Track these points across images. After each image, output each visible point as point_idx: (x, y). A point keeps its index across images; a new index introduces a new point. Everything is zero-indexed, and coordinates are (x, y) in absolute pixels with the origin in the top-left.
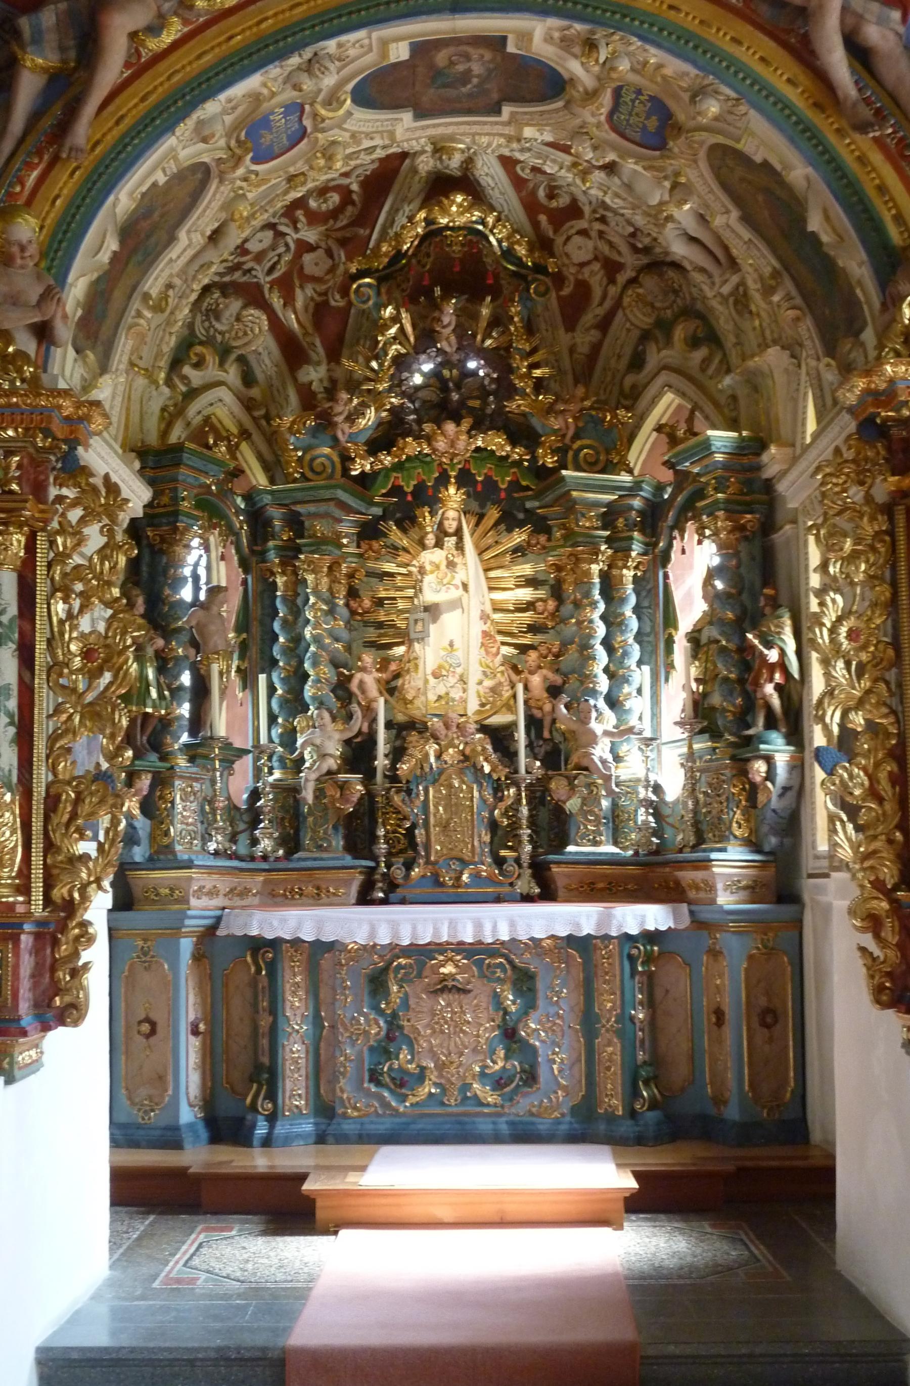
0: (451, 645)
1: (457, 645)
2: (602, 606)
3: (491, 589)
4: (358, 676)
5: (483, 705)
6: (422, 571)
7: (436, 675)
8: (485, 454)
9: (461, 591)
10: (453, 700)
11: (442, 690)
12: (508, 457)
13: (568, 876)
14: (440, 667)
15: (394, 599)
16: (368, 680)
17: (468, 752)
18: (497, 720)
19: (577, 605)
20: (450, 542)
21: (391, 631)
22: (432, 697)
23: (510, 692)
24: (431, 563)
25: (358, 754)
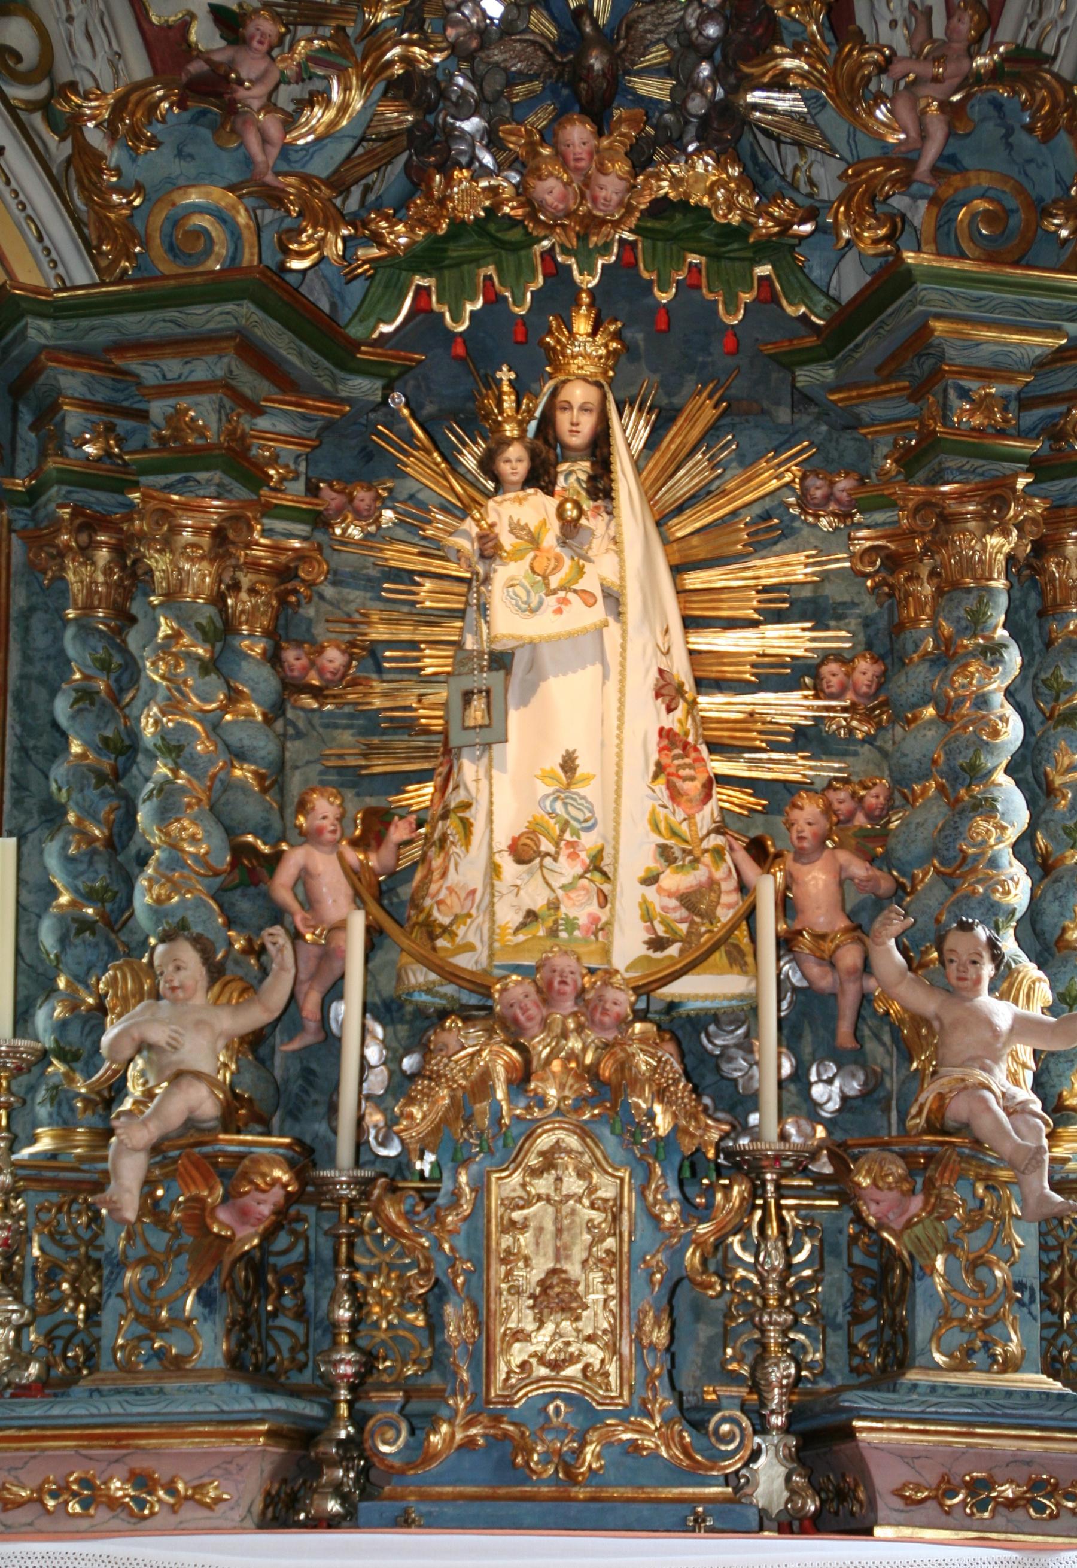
0: (569, 764)
1: (584, 766)
2: (1013, 658)
3: (690, 623)
4: (295, 858)
5: (657, 944)
6: (489, 549)
7: (523, 852)
8: (680, 222)
9: (598, 612)
10: (571, 925)
11: (536, 897)
12: (747, 227)
13: (908, 1456)
14: (533, 831)
15: (414, 645)
16: (321, 871)
17: (607, 1071)
18: (703, 988)
19: (947, 657)
20: (573, 475)
21: (401, 741)
22: (508, 915)
23: (742, 906)
24: (516, 528)
25: (282, 1077)
